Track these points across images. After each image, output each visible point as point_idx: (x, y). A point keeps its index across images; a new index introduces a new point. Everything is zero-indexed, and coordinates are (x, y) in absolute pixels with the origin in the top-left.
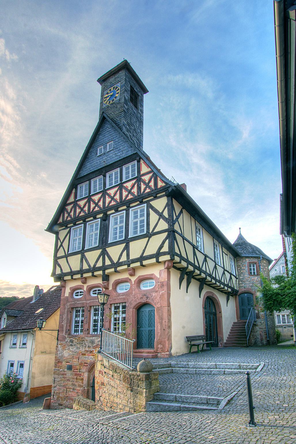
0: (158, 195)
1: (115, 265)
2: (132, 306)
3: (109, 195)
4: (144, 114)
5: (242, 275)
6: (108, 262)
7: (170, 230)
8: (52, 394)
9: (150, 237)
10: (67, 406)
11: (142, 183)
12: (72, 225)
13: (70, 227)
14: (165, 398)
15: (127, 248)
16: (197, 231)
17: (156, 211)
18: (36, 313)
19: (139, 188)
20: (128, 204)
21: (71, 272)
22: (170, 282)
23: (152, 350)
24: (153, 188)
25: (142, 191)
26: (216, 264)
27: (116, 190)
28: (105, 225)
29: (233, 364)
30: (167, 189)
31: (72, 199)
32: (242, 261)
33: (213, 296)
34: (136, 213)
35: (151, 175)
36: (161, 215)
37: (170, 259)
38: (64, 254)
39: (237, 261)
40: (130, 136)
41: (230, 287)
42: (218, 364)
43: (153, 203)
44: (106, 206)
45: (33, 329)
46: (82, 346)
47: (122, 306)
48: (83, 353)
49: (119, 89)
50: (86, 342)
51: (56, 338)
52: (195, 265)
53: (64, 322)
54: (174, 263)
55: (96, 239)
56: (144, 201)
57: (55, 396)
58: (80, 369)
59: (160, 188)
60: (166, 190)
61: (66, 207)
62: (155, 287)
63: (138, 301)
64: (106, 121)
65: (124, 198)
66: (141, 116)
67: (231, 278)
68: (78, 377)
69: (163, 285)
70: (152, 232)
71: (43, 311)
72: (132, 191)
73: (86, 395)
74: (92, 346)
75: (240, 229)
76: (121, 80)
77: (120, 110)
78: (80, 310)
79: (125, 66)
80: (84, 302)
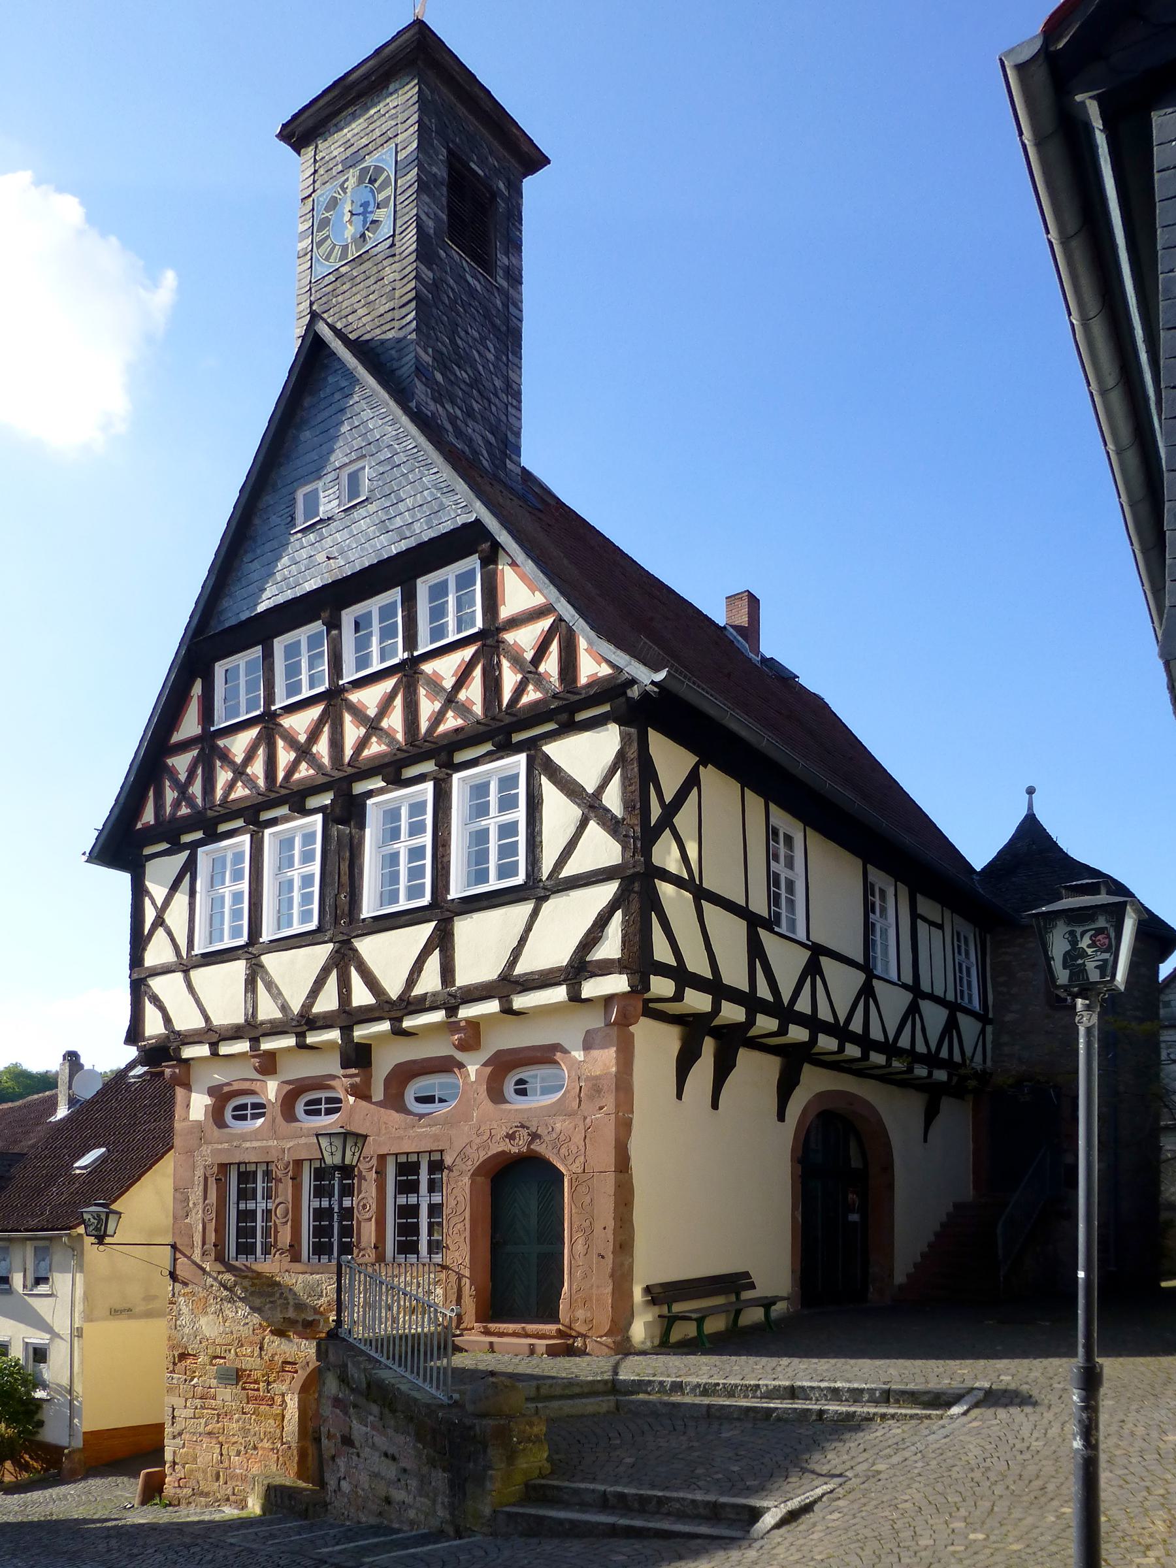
0: (581, 716)
1: (397, 1009)
2: (470, 1167)
3: (358, 713)
4: (526, 288)
6: (361, 996)
8: (168, 1456)
12: (199, 835)
13: (194, 846)
14: (566, 1497)
15: (443, 941)
17: (570, 788)
19: (492, 685)
20: (444, 754)
22: (631, 1075)
23: (551, 1328)
27: (389, 690)
31: (190, 726)
34: (480, 790)
35: (546, 623)
36: (591, 806)
40: (452, 419)
41: (948, 1064)
43: (555, 750)
44: (347, 759)
45: (70, 1228)
46: (271, 1302)
47: (430, 1161)
55: (307, 898)
56: (517, 738)
59: (589, 685)
61: (170, 761)
63: (495, 1149)
70: (550, 877)
71: (102, 1160)
72: (462, 696)
75: (1031, 791)
76: (401, 128)
78: (255, 1173)
79: (418, 55)
80: (270, 1143)
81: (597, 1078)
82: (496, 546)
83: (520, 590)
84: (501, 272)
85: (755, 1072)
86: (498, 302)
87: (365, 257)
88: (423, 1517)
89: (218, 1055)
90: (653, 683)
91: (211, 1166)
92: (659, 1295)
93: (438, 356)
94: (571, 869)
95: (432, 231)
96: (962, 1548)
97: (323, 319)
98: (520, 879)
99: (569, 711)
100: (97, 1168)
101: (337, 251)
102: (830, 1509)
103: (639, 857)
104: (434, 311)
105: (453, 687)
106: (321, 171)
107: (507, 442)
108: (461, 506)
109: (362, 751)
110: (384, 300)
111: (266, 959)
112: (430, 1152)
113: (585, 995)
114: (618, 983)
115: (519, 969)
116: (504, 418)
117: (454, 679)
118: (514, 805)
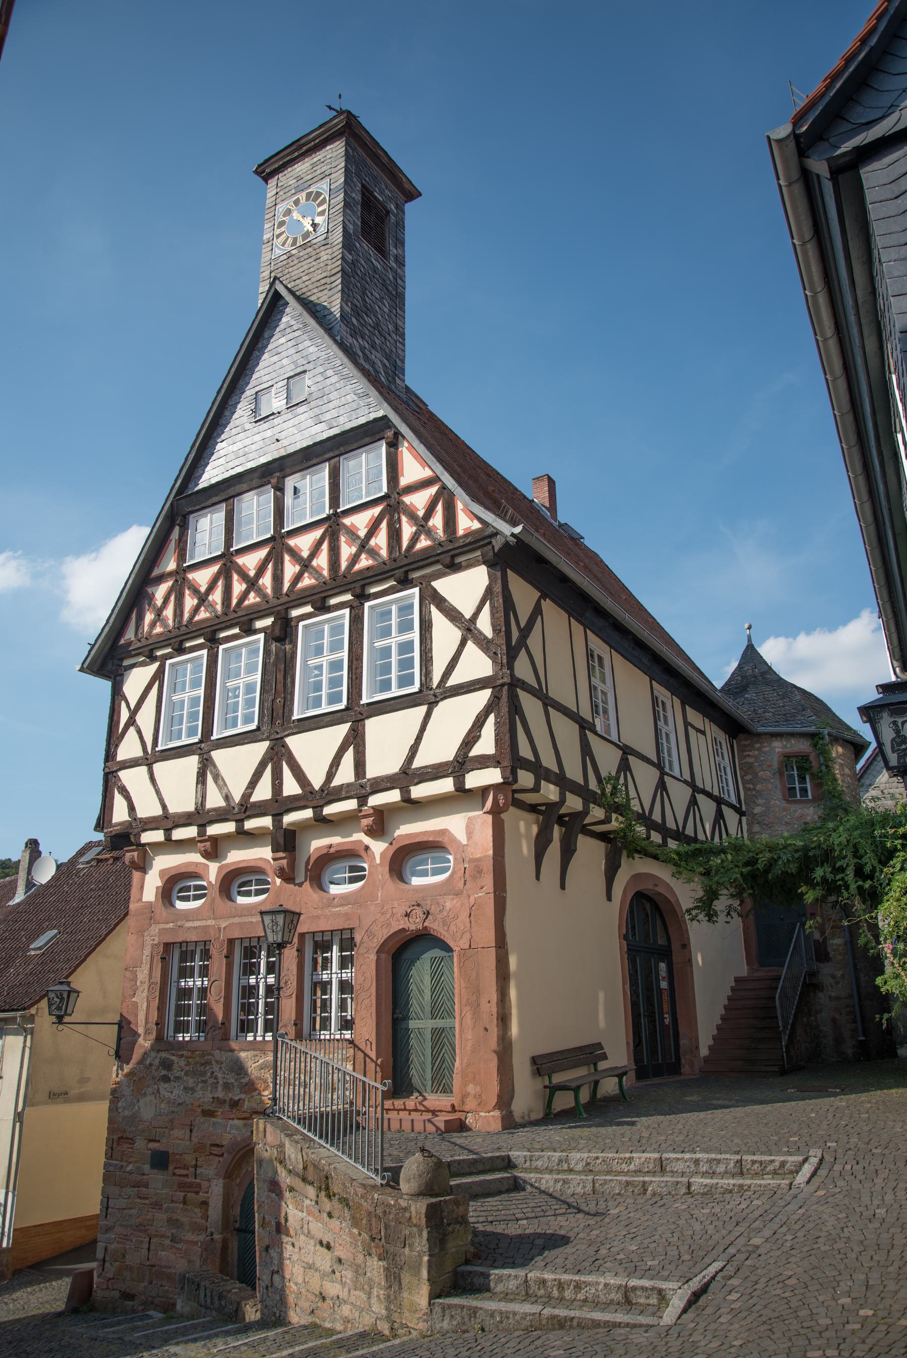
2: (376, 943)
3: (294, 554)
4: (407, 269)
5: (760, 801)
7: (500, 682)
9: (432, 705)
10: (152, 1303)
11: (404, 519)
15: (356, 740)
16: (594, 667)
17: (453, 615)
18: (31, 947)
19: (395, 535)
20: (359, 586)
21: (166, 815)
24: (442, 534)
25: (405, 543)
26: (663, 774)
27: (318, 537)
28: (281, 655)
29: (719, 1156)
30: (486, 541)
32: (759, 749)
33: (657, 889)
35: (433, 490)
36: (468, 629)
37: (502, 780)
38: (140, 753)
39: (742, 749)
42: (667, 1159)
45: (24, 1009)
46: (203, 1082)
48: (206, 1108)
49: (325, 198)
50: (216, 1068)
51: (112, 1052)
52: (588, 790)
53: (138, 992)
54: (514, 791)
55: (249, 703)
57: (107, 1265)
58: (196, 1166)
59: (466, 536)
60: (485, 545)
61: (150, 590)
62: (452, 875)
63: (396, 927)
64: (283, 305)
65: (344, 565)
66: (399, 277)
67: (719, 815)
68: (189, 1195)
69: (480, 872)
72: (372, 542)
73: (218, 1260)
74: (236, 1084)
76: (333, 170)
77: (329, 268)
81: (478, 860)
82: (397, 434)
83: (413, 469)
84: (392, 259)
85: (591, 853)
86: (391, 277)
87: (309, 244)
88: (357, 1314)
89: (171, 840)
90: (513, 535)
91: (158, 945)
92: (542, 1065)
93: (354, 308)
94: (455, 680)
95: (352, 231)
96: (858, 1326)
97: (281, 282)
98: (415, 688)
99: (451, 556)
100: (49, 952)
101: (290, 241)
102: (727, 1288)
103: (505, 670)
104: (352, 279)
105: (366, 536)
106: (281, 193)
107: (396, 368)
108: (371, 408)
109: (297, 584)
110: (320, 271)
111: (217, 755)
112: (342, 930)
113: (468, 786)
114: (492, 776)
115: (417, 763)
116: (394, 350)
117: (366, 530)
118: (411, 628)
